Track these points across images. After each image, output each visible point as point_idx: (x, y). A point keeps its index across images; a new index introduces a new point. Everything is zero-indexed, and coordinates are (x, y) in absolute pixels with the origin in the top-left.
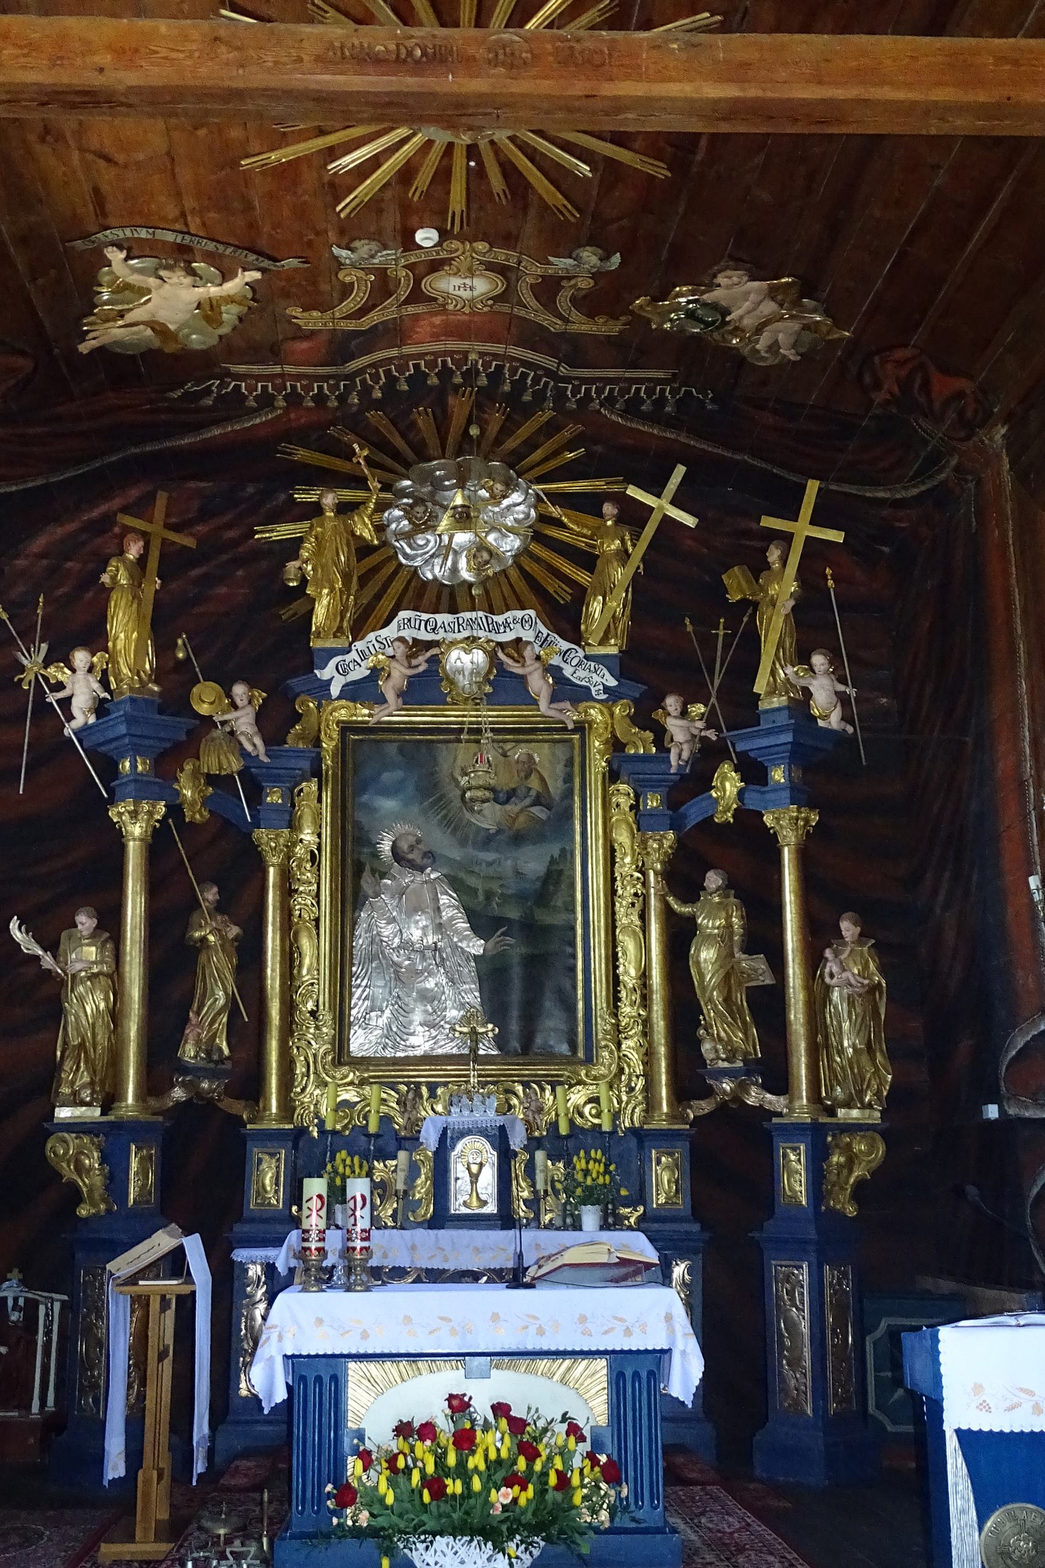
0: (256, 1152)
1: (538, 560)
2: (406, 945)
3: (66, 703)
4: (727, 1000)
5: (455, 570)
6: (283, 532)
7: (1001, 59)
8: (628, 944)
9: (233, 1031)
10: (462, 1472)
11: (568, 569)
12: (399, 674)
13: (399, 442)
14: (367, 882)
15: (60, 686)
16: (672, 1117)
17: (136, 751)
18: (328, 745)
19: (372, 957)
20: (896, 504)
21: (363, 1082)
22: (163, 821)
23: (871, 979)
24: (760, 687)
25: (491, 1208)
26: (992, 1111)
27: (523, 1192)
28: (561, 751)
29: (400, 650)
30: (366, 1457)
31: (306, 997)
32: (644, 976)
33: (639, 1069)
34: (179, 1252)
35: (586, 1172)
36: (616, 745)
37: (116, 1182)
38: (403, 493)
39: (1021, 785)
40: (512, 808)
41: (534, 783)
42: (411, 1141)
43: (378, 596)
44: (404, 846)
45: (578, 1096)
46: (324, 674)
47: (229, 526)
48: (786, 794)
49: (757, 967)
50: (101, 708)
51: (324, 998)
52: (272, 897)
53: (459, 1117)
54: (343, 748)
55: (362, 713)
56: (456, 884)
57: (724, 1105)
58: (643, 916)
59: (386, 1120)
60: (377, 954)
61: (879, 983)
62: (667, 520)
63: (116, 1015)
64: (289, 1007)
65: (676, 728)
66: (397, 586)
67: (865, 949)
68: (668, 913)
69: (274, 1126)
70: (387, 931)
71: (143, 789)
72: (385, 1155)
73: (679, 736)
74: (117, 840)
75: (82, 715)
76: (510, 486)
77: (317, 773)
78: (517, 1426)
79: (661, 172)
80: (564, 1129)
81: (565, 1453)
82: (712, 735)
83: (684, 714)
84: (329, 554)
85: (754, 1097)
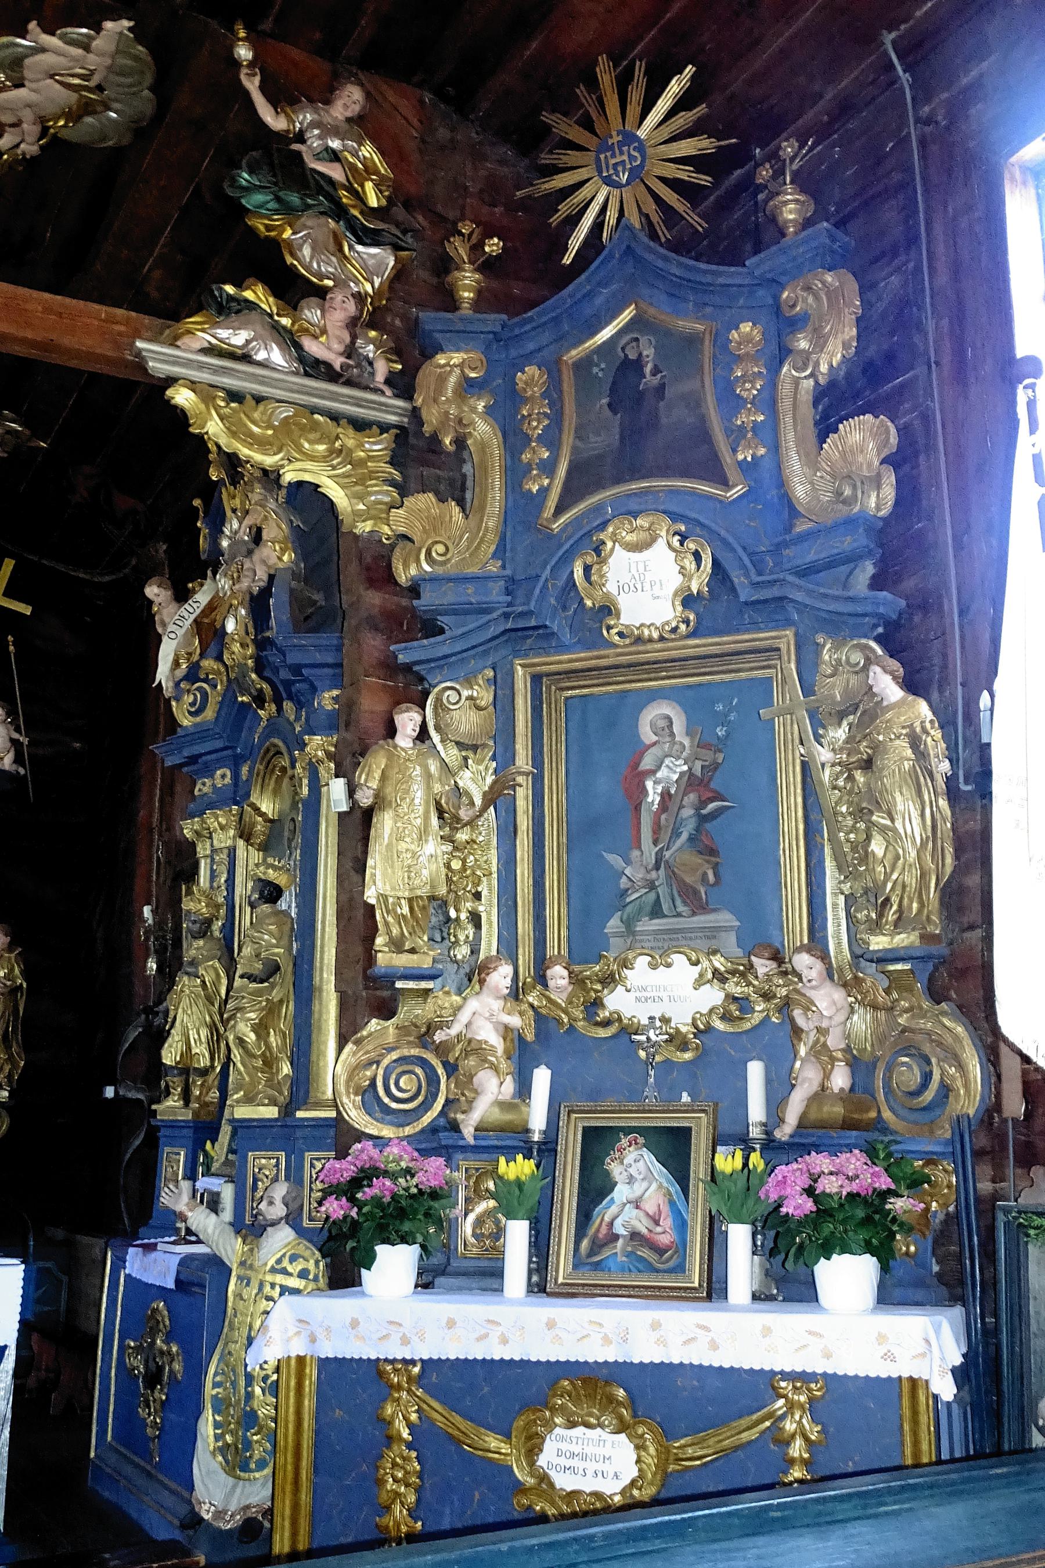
7: (48, 310)
23: (14, 982)
26: (110, 1092)
39: (151, 831)
61: (21, 984)
67: (13, 955)
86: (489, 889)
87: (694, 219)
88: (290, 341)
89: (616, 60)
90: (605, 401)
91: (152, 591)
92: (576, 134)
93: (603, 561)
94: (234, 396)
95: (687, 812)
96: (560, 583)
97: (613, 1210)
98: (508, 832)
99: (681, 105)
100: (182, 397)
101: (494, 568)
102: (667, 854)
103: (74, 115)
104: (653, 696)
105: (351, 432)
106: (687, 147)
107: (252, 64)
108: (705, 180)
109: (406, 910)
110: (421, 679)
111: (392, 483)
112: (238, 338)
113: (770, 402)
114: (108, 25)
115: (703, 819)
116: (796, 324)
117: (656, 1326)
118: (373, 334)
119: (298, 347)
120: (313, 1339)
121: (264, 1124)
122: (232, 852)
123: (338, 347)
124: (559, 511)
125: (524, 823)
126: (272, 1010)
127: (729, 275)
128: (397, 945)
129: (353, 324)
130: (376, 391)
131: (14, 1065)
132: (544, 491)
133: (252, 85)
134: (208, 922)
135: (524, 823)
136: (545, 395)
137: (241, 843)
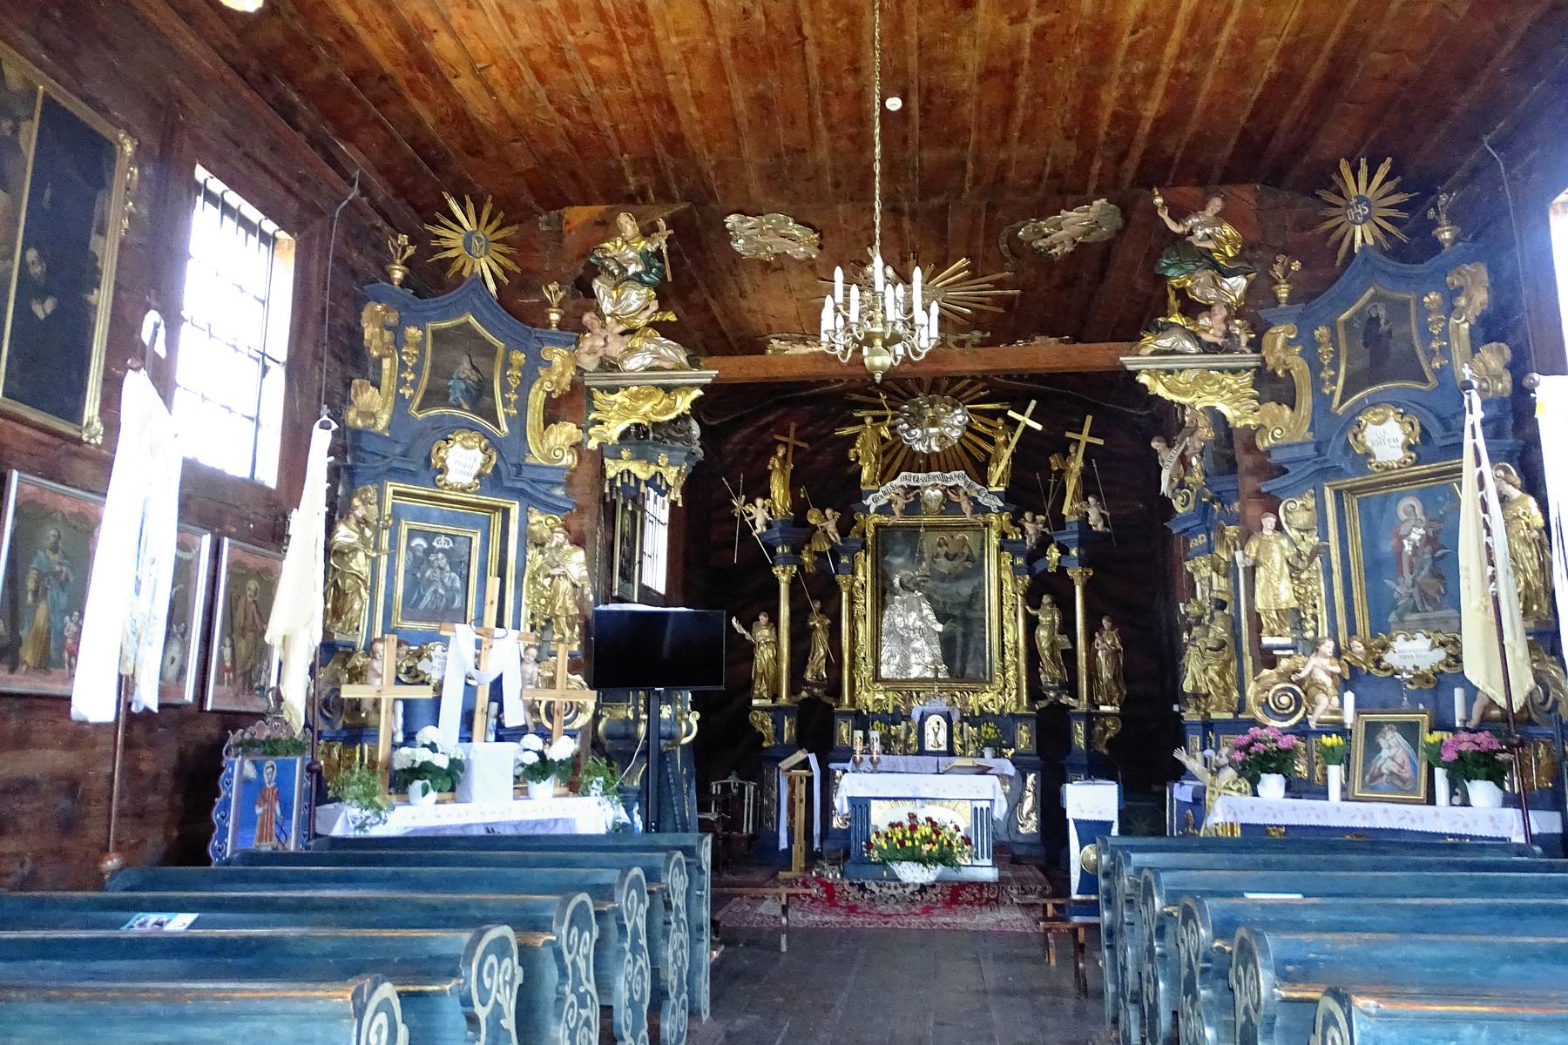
0: (839, 720)
1: (970, 441)
2: (906, 627)
3: (753, 522)
4: (1052, 656)
5: (929, 446)
6: (848, 431)
8: (1009, 627)
9: (828, 665)
10: (912, 839)
11: (984, 445)
12: (901, 502)
13: (899, 390)
14: (888, 596)
15: (751, 514)
16: (1028, 709)
17: (784, 543)
18: (869, 535)
19: (890, 633)
20: (1139, 416)
21: (886, 690)
22: (796, 574)
24: (1065, 511)
25: (944, 748)
27: (957, 741)
28: (978, 536)
29: (901, 491)
30: (878, 834)
31: (860, 651)
32: (1016, 642)
33: (1014, 686)
34: (807, 760)
35: (986, 732)
36: (1003, 535)
37: (779, 733)
38: (904, 411)
40: (955, 563)
41: (966, 551)
42: (908, 718)
43: (894, 459)
44: (905, 580)
45: (985, 698)
46: (868, 502)
47: (823, 427)
48: (1076, 562)
49: (1063, 640)
50: (768, 525)
51: (869, 652)
52: (845, 606)
53: (927, 708)
54: (876, 537)
55: (884, 519)
56: (929, 598)
57: (1051, 704)
58: (1016, 615)
59: (896, 708)
60: (893, 631)
62: (1027, 428)
63: (777, 659)
64: (853, 656)
65: (1029, 527)
66: (902, 454)
68: (1026, 613)
69: (847, 709)
70: (898, 620)
71: (787, 561)
72: (896, 723)
73: (1031, 531)
74: (775, 582)
75: (760, 528)
76: (955, 406)
77: (864, 547)
78: (934, 824)
79: (1001, 310)
80: (977, 714)
81: (952, 836)
82: (1046, 530)
83: (1034, 520)
84: (869, 444)
85: (1064, 700)
86: (1321, 603)
87: (1401, 237)
88: (1195, 337)
89: (1349, 159)
90: (1361, 341)
91: (1154, 444)
92: (1334, 199)
93: (1362, 431)
94: (1169, 372)
95: (1427, 556)
96: (1342, 443)
97: (1381, 762)
98: (1328, 572)
99: (1388, 178)
100: (1144, 379)
101: (1309, 436)
102: (1418, 579)
103: (1085, 234)
104: (1402, 495)
105: (1230, 376)
106: (1395, 199)
107: (1164, 205)
108: (1405, 215)
109: (1275, 617)
110: (1276, 498)
111: (1254, 397)
112: (1165, 343)
113: (1445, 335)
114: (1096, 203)
115: (1435, 560)
116: (1458, 291)
117: (1386, 811)
118: (1237, 322)
119: (1199, 339)
120: (1235, 814)
121: (1227, 721)
122: (1210, 579)
123: (1220, 334)
124: (1342, 402)
125: (1336, 567)
126: (1226, 664)
127: (1418, 269)
128: (1272, 634)
129: (1226, 320)
130: (1242, 352)
131: (1121, 693)
132: (1333, 393)
133: (1164, 215)
134: (1201, 617)
135: (1336, 567)
136: (1331, 341)
137: (1214, 574)
